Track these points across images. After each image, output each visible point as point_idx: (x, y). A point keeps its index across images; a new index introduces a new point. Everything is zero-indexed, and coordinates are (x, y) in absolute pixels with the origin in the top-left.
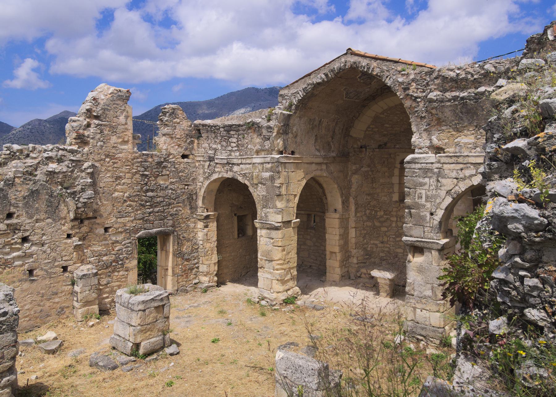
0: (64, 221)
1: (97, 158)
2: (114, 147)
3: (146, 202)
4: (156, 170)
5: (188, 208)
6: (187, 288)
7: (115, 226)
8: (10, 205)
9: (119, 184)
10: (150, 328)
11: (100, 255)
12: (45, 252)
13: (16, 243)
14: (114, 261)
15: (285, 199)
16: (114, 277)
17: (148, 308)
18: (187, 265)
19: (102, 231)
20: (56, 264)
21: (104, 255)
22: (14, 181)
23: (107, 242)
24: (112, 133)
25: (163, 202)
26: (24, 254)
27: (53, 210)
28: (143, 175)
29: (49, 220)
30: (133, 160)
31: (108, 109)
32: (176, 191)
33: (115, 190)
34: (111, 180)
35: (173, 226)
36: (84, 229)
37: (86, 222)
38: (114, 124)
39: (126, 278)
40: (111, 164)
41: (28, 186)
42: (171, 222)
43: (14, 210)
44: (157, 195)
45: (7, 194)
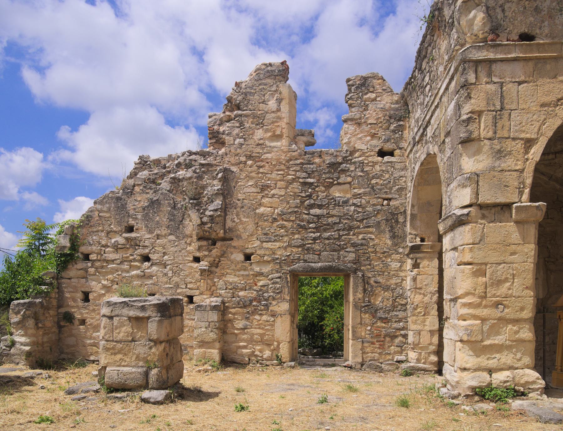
0: (189, 239)
1: (233, 160)
2: (258, 145)
3: (309, 223)
4: (328, 175)
5: (388, 236)
6: (383, 366)
7: (259, 252)
8: (129, 216)
9: (267, 196)
10: (122, 349)
11: (235, 288)
12: (166, 274)
13: (134, 260)
14: (255, 299)
15: (486, 148)
16: (254, 321)
17: (117, 316)
18: (384, 328)
19: (241, 257)
20: (179, 291)
21: (242, 290)
22: (133, 189)
23: (246, 273)
24: (257, 125)
25: (339, 223)
26: (142, 274)
27: (176, 225)
28: (304, 184)
29: (172, 237)
30: (288, 161)
31: (251, 93)
32: (363, 208)
33: (260, 205)
34: (254, 190)
35: (356, 261)
36: (215, 252)
37: (219, 244)
38: (259, 113)
39: (273, 326)
40: (255, 168)
41: (148, 196)
42: (353, 255)
43: (133, 222)
44: (328, 214)
45: (126, 204)
